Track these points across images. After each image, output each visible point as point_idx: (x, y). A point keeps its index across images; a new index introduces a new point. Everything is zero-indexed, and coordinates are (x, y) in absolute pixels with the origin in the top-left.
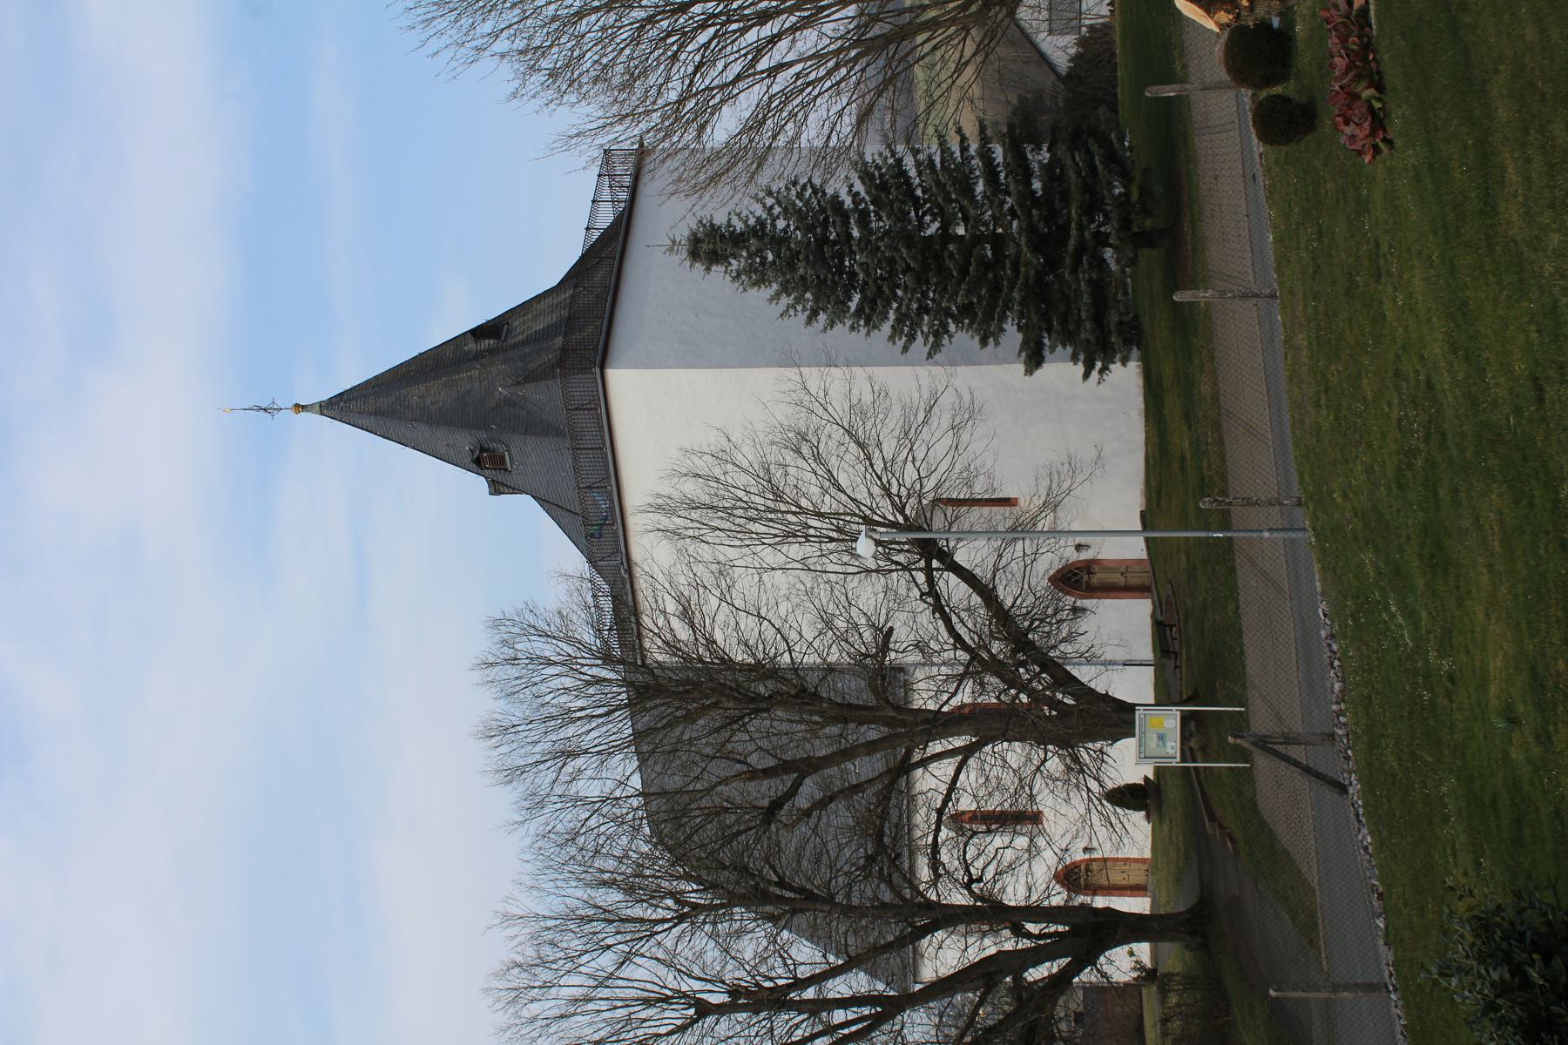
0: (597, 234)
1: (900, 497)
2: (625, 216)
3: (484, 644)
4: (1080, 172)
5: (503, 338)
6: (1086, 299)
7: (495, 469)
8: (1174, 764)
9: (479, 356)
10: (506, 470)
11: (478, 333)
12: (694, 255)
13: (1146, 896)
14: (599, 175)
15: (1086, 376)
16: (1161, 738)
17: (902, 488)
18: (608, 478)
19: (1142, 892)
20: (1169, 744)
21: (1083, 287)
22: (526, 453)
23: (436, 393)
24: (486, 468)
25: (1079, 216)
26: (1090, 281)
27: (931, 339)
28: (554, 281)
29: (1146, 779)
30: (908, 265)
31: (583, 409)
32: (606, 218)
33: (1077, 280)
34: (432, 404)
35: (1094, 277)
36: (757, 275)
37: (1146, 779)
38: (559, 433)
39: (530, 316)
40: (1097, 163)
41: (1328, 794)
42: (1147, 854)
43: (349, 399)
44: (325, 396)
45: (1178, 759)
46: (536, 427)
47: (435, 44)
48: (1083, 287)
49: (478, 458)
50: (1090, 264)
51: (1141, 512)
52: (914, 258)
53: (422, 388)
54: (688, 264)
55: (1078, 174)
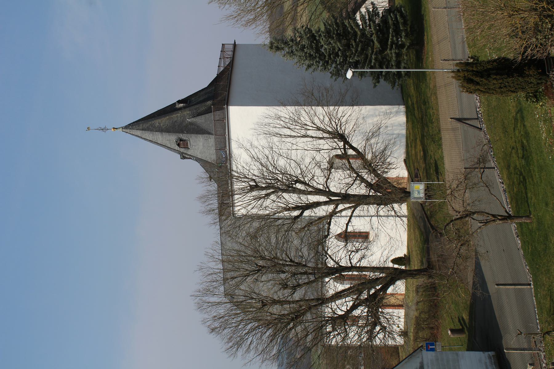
0: (222, 69)
1: (336, 123)
4: (392, 19)
5: (188, 103)
6: (394, 59)
7: (184, 148)
8: (423, 200)
9: (180, 109)
10: (188, 148)
11: (179, 102)
12: (271, 48)
13: (403, 309)
16: (419, 193)
17: (336, 120)
18: (225, 147)
19: (402, 308)
21: (393, 55)
23: (164, 121)
24: (181, 147)
25: (392, 32)
26: (395, 53)
28: (206, 86)
29: (405, 255)
30: (339, 48)
31: (221, 121)
33: (391, 53)
34: (163, 126)
35: (397, 51)
37: (405, 255)
38: (209, 133)
39: (197, 97)
40: (398, 16)
41: (477, 131)
42: (404, 292)
43: (132, 125)
44: (124, 125)
45: (424, 199)
48: (393, 55)
49: (179, 143)
51: (404, 159)
52: (341, 46)
53: (159, 120)
55: (392, 20)
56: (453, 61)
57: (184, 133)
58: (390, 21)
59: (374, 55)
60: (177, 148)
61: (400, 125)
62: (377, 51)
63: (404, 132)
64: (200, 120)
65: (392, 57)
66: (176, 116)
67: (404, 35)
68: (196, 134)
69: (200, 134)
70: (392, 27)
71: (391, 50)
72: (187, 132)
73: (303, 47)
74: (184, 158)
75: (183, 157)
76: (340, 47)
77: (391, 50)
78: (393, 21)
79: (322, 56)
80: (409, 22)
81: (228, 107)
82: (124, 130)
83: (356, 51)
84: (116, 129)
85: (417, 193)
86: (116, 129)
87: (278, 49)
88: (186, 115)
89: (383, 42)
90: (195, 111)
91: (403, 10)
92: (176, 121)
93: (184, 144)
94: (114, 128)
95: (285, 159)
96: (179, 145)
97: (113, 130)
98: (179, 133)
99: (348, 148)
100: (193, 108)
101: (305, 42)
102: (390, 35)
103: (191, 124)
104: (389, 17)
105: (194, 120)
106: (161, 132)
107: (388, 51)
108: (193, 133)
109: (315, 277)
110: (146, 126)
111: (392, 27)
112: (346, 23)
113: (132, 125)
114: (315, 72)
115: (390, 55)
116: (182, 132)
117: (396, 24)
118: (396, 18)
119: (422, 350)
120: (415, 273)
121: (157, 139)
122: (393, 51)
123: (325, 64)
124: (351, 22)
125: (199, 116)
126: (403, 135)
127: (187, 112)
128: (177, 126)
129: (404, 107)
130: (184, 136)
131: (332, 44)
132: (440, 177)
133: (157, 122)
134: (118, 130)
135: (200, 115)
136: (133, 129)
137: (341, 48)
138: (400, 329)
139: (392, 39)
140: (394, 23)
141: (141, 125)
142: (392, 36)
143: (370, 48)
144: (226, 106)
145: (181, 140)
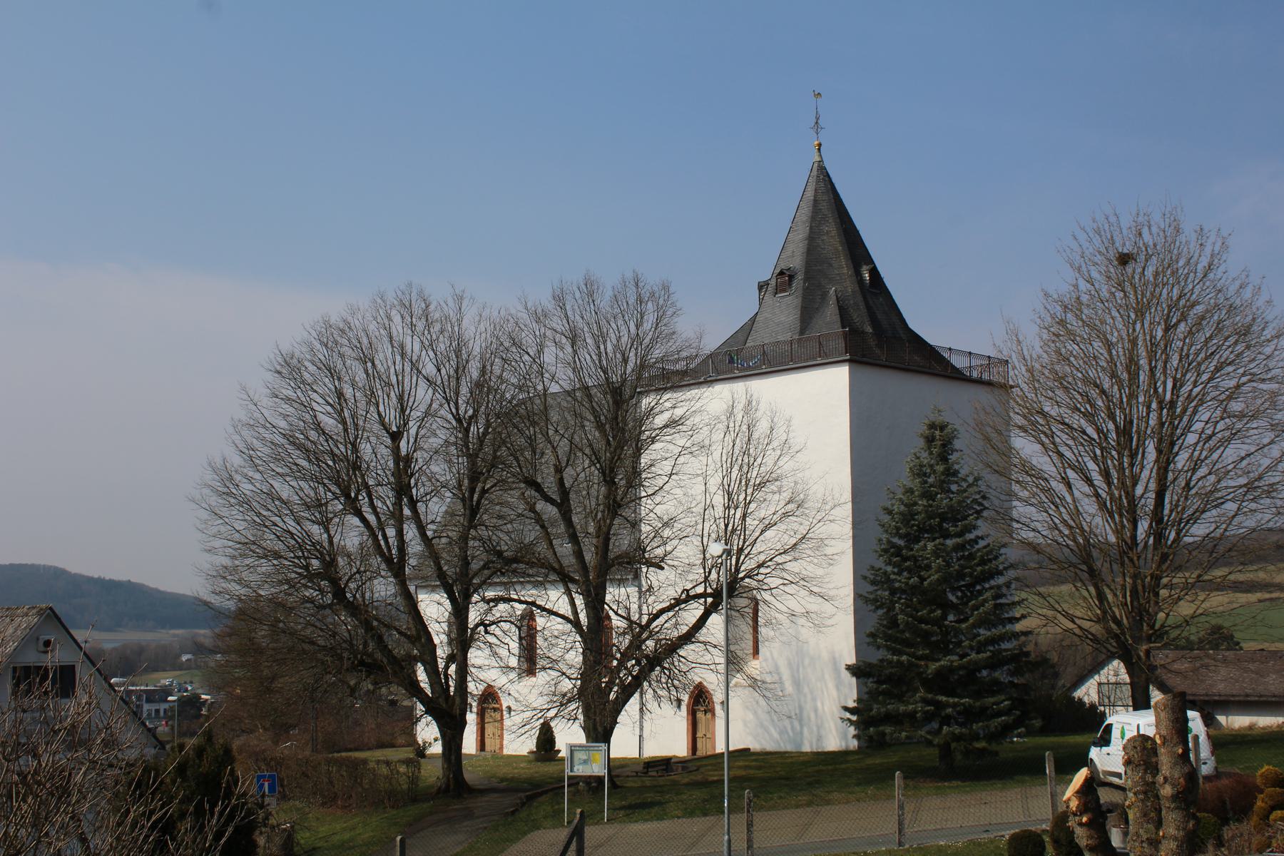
0: (946, 355)
2: (961, 376)
3: (924, 429)
6: (902, 708)
9: (858, 273)
10: (776, 293)
11: (874, 272)
12: (932, 426)
13: (477, 750)
14: (989, 357)
15: (846, 709)
16: (585, 762)
20: (581, 767)
21: (911, 707)
22: (785, 312)
23: (832, 240)
26: (915, 712)
27: (872, 597)
28: (911, 326)
32: (959, 362)
34: (823, 240)
36: (920, 472)
37: (559, 751)
38: (802, 332)
40: (1003, 718)
42: (506, 752)
44: (827, 165)
46: (807, 314)
47: (1082, 237)
48: (911, 707)
49: (784, 274)
50: (928, 711)
52: (930, 584)
53: (834, 233)
54: (927, 422)
56: (748, 825)
57: (804, 283)
58: (992, 700)
59: (908, 660)
60: (778, 271)
61: (819, 738)
62: (918, 666)
63: (807, 748)
64: (830, 313)
65: (908, 703)
66: (842, 266)
67: (957, 732)
68: (802, 307)
69: (802, 314)
70: (978, 704)
71: (925, 701)
72: (807, 288)
73: (931, 497)
74: (761, 287)
75: (762, 286)
76: (928, 580)
77: (925, 701)
78: (992, 707)
79: (912, 539)
80: (994, 747)
81: (847, 364)
82: (816, 165)
83: (921, 621)
84: (819, 149)
85: (585, 757)
86: (819, 149)
87: (930, 440)
88: (841, 282)
89: (942, 682)
90: (852, 302)
91: (1019, 731)
92: (831, 265)
93: (782, 283)
94: (820, 145)
95: (423, 372)
96: (781, 273)
97: (816, 143)
98: (807, 272)
99: (705, 602)
100: (860, 298)
101: (943, 501)
102: (956, 700)
103: (824, 295)
104: (1003, 697)
105: (832, 301)
106: (810, 237)
107: (921, 693)
108: (804, 298)
109: (432, 539)
110: (825, 207)
111: (978, 704)
112: (988, 595)
113: (825, 181)
114: (880, 529)
115: (911, 701)
116: (806, 279)
117: (984, 714)
118: (999, 714)
119: (155, 748)
120: (453, 757)
121: (796, 231)
122: (919, 706)
123: (892, 550)
124: (987, 605)
125: (839, 309)
126: (801, 744)
127: (850, 286)
128: (820, 268)
129: (854, 747)
130: (798, 282)
131: (935, 562)
132: (622, 813)
133: (831, 229)
134: (816, 154)
135: (840, 312)
136: (818, 182)
137: (926, 583)
138: (430, 743)
139: (947, 705)
140: (987, 708)
141: (825, 197)
142: (954, 705)
143: (928, 652)
144: (848, 357)
145: (791, 277)
